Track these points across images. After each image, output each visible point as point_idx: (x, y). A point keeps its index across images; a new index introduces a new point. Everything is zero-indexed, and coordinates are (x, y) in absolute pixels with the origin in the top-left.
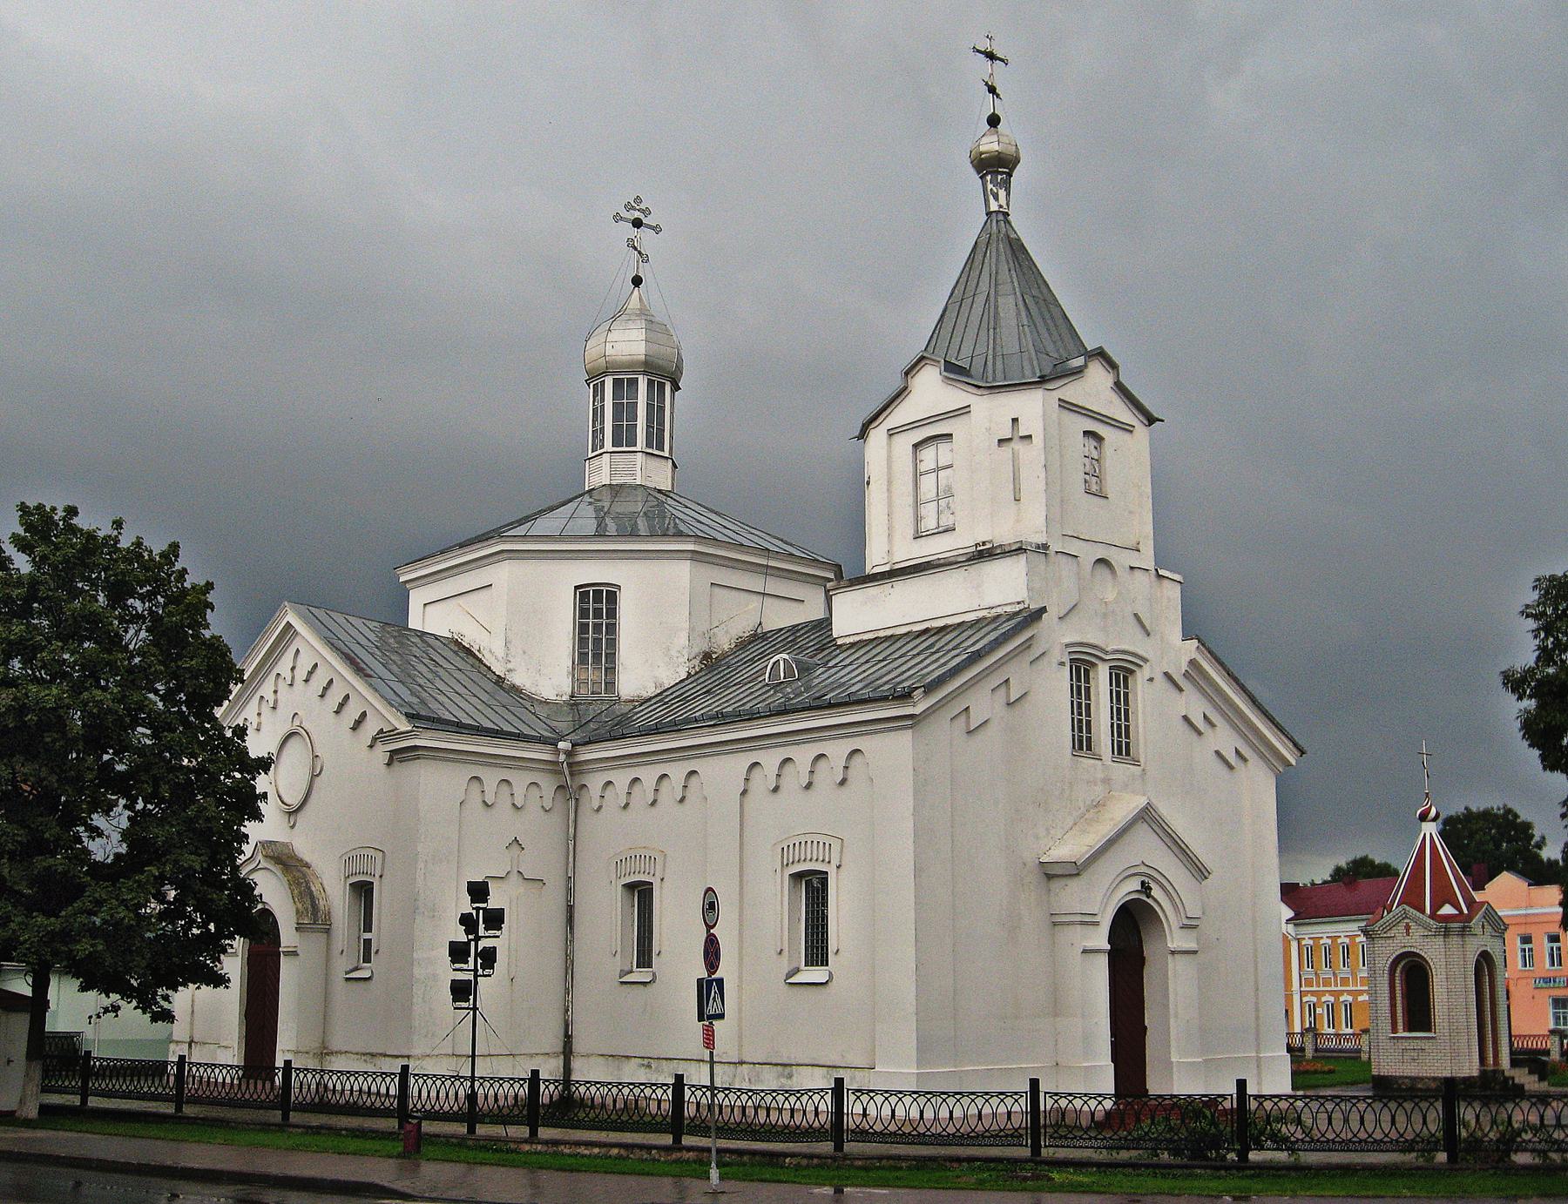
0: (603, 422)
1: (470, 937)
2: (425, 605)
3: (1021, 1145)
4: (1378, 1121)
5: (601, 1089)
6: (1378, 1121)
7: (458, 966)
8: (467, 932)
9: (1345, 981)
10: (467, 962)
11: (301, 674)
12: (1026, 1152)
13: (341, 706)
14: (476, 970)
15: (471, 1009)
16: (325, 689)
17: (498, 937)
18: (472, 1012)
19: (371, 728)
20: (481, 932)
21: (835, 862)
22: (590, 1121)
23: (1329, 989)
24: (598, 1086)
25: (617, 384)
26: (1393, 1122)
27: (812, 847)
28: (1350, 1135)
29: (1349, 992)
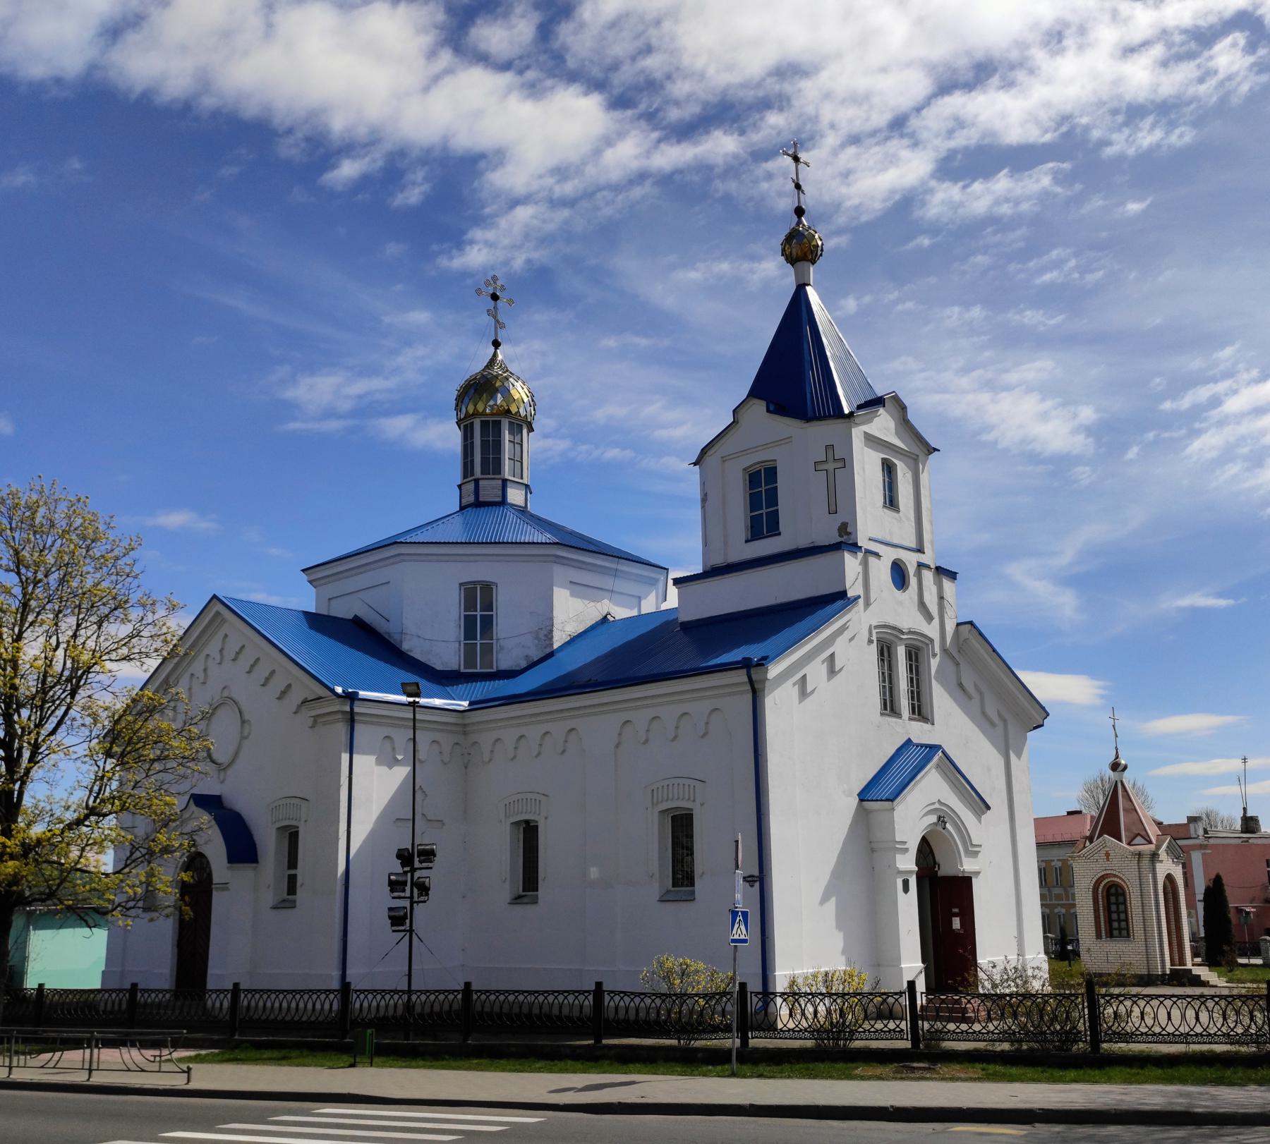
0: (472, 455)
1: (406, 869)
2: (330, 599)
3: (902, 1039)
4: (1183, 1016)
5: (529, 998)
6: (1183, 1016)
7: (396, 894)
8: (403, 865)
9: (1058, 897)
10: (404, 891)
11: (230, 652)
12: (908, 1045)
13: (267, 680)
14: (411, 897)
15: (407, 931)
16: (252, 666)
17: (431, 868)
18: (408, 934)
19: (296, 697)
20: (417, 864)
21: (698, 801)
22: (1001, 1033)
23: (1061, 902)
24: (526, 994)
25: (484, 424)
26: (1197, 1019)
27: (678, 789)
28: (1187, 1029)
29: (1062, 906)
